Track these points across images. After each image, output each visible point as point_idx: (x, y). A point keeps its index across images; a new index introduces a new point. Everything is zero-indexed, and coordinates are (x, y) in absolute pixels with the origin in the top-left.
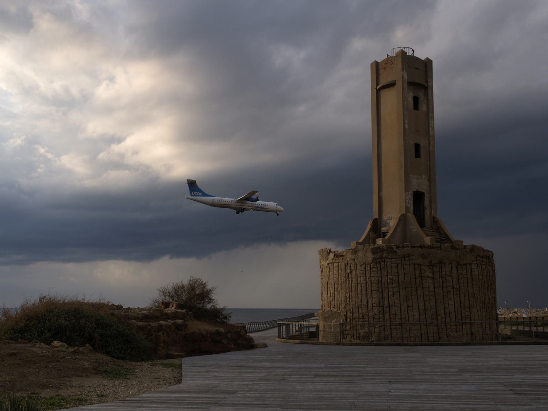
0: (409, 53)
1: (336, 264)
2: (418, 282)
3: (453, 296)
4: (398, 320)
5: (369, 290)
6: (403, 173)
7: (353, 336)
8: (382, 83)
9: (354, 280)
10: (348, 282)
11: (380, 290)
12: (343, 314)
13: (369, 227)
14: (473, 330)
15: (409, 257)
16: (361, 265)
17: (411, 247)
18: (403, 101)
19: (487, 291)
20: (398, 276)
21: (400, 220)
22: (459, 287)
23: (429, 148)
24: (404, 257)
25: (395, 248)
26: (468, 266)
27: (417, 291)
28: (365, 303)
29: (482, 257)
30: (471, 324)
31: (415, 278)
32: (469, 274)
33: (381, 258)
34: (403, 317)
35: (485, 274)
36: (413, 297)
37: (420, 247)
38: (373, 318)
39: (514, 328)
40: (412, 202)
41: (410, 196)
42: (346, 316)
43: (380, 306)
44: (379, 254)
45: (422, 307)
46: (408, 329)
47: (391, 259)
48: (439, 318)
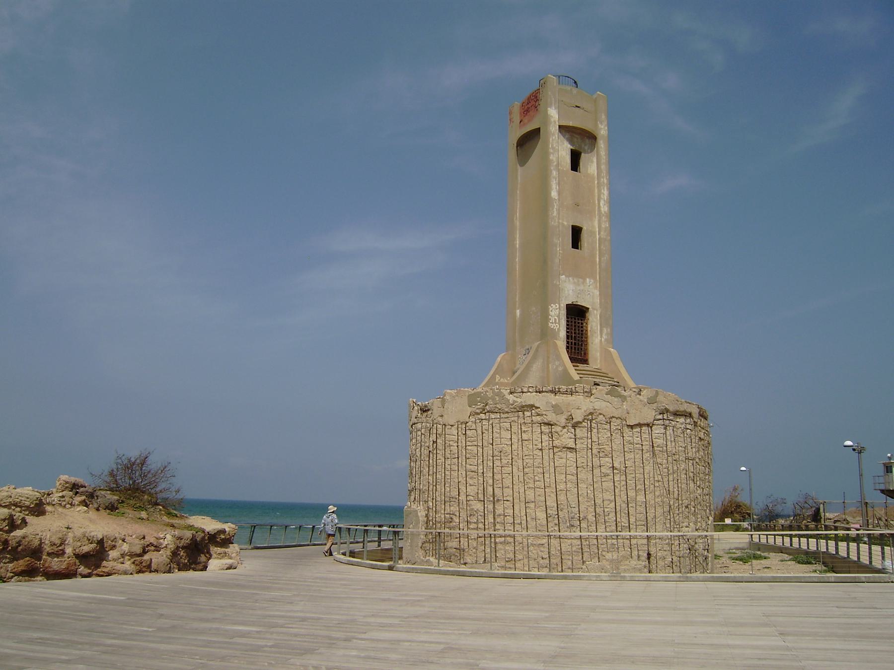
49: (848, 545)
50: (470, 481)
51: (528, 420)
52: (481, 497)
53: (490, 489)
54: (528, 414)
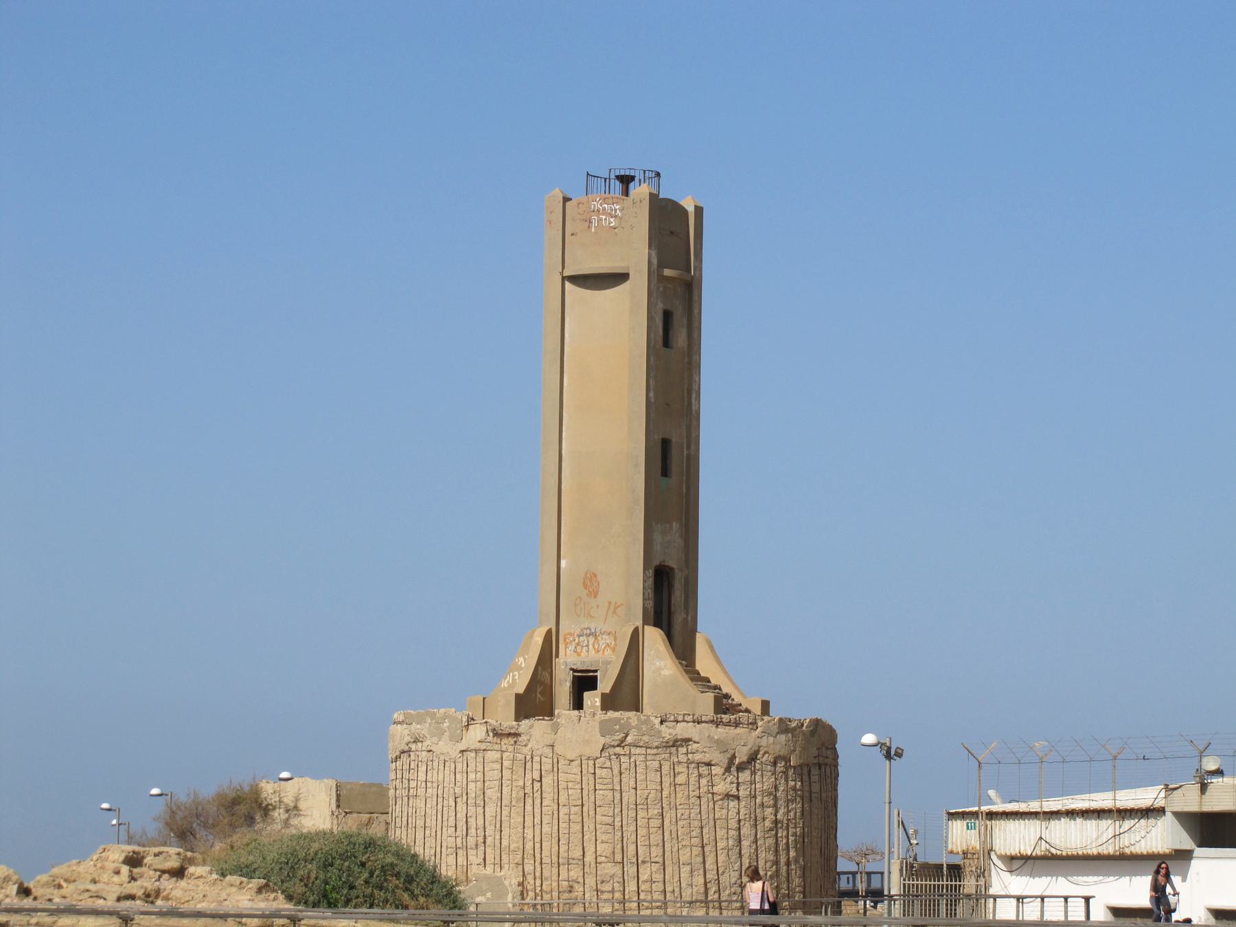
11: (618, 824)
49: (1066, 916)
50: (601, 837)
51: (683, 758)
52: (618, 857)
53: (632, 848)
54: (683, 750)
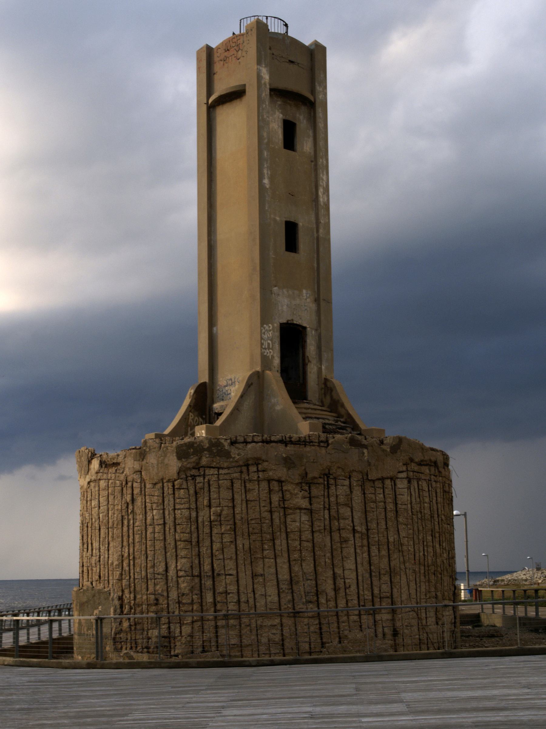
0: (275, 27)
1: (103, 484)
2: (277, 521)
3: (353, 550)
4: (232, 607)
5: (170, 540)
6: (257, 284)
7: (134, 645)
8: (220, 89)
9: (140, 517)
10: (126, 522)
11: (194, 540)
12: (115, 595)
13: (187, 401)
14: (398, 624)
15: (257, 465)
16: (155, 484)
17: (263, 442)
18: (260, 128)
19: (429, 538)
20: (234, 507)
21: (249, 385)
22: (368, 530)
23: (318, 231)
24: (247, 466)
25: (226, 444)
26: (388, 482)
27: (273, 540)
28: (161, 569)
29: (420, 464)
30: (394, 611)
31: (271, 512)
32: (389, 500)
33: (197, 467)
34: (243, 599)
35: (427, 500)
36: (265, 553)
37: (281, 441)
38: (179, 602)
39: (510, 611)
40: (277, 347)
41: (272, 334)
42: (121, 598)
43: (193, 576)
44: (193, 459)
45: (284, 575)
46: (254, 625)
47: (219, 468)
48: (323, 600)
49: (526, 613)
